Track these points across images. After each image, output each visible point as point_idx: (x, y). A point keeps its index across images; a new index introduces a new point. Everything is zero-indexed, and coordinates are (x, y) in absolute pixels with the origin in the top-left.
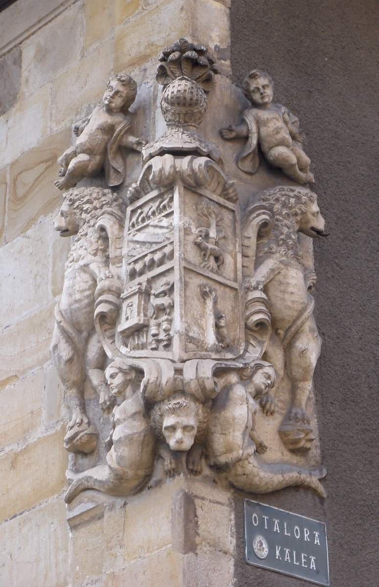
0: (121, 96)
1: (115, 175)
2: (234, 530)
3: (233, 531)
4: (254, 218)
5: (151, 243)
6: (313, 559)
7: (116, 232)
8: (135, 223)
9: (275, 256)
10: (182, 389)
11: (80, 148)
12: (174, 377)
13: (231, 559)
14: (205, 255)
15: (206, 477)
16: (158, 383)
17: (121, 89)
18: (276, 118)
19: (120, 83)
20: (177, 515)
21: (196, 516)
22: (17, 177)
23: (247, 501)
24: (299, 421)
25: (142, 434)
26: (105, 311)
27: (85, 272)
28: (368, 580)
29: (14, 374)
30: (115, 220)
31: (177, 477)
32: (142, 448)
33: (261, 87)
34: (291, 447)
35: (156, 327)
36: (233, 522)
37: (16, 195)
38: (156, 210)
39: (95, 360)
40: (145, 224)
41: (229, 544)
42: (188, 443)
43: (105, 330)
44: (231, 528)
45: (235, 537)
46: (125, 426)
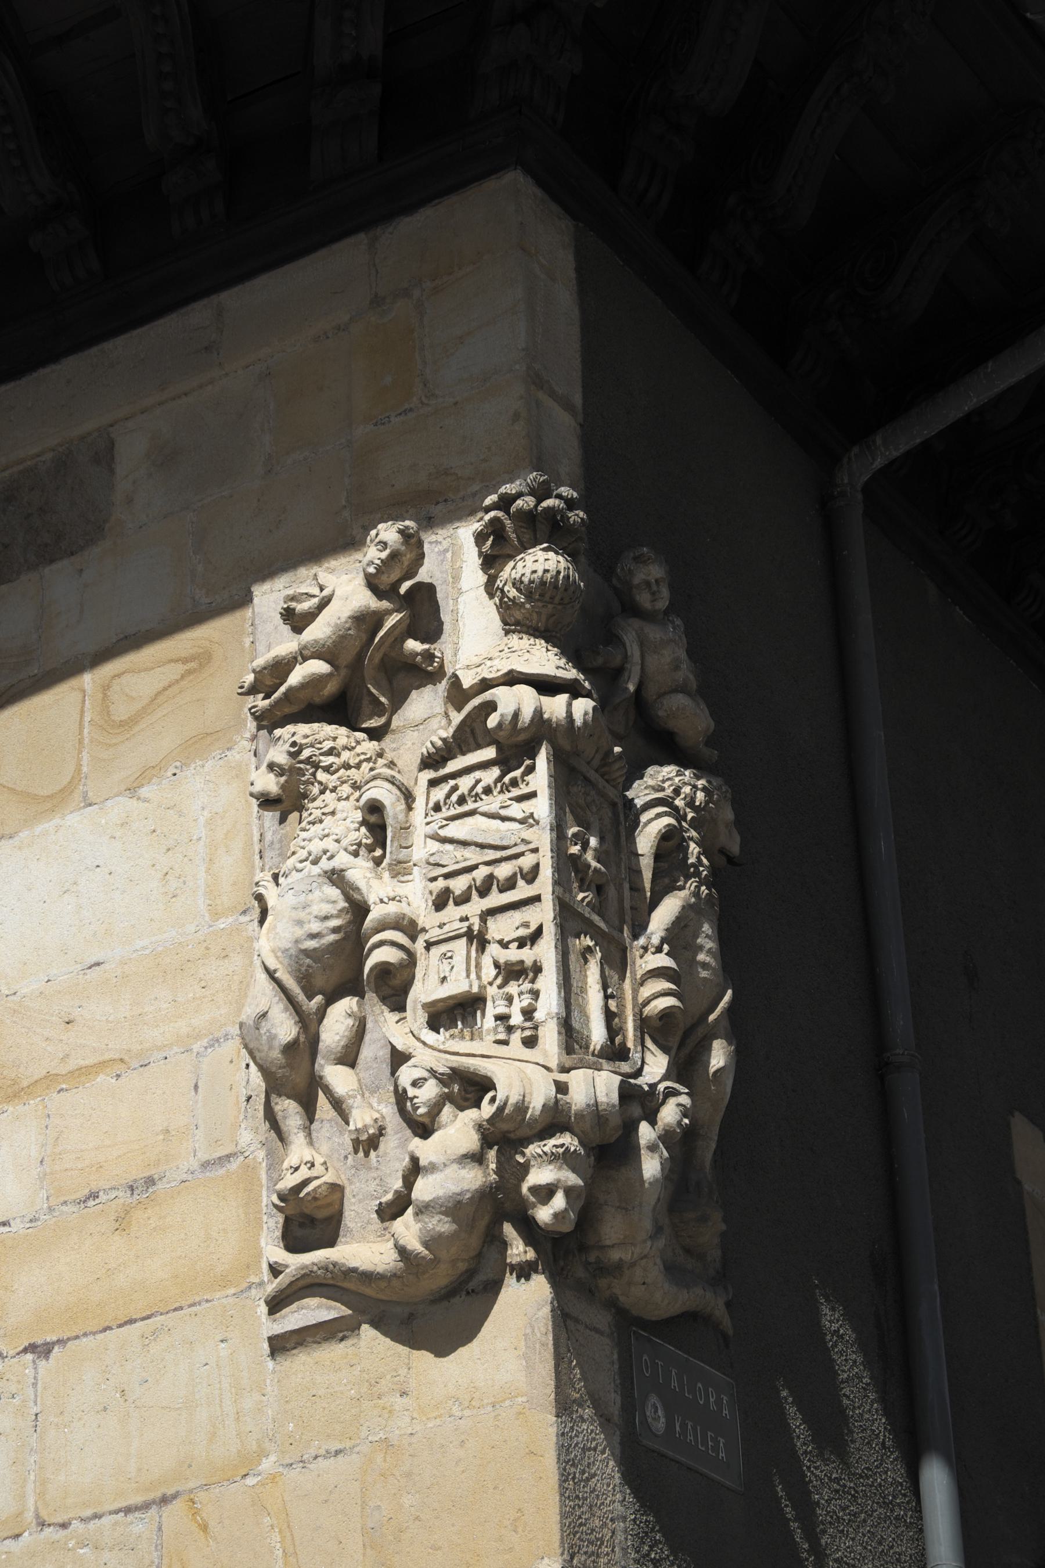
5: (482, 846)
6: (722, 1441)
7: (401, 817)
8: (442, 803)
12: (556, 1097)
13: (616, 1431)
20: (537, 1346)
26: (392, 961)
30: (398, 793)
35: (506, 1003)
36: (616, 1366)
38: (493, 785)
39: (339, 1049)
40: (466, 808)
41: (613, 1405)
44: (614, 1378)
45: (619, 1393)
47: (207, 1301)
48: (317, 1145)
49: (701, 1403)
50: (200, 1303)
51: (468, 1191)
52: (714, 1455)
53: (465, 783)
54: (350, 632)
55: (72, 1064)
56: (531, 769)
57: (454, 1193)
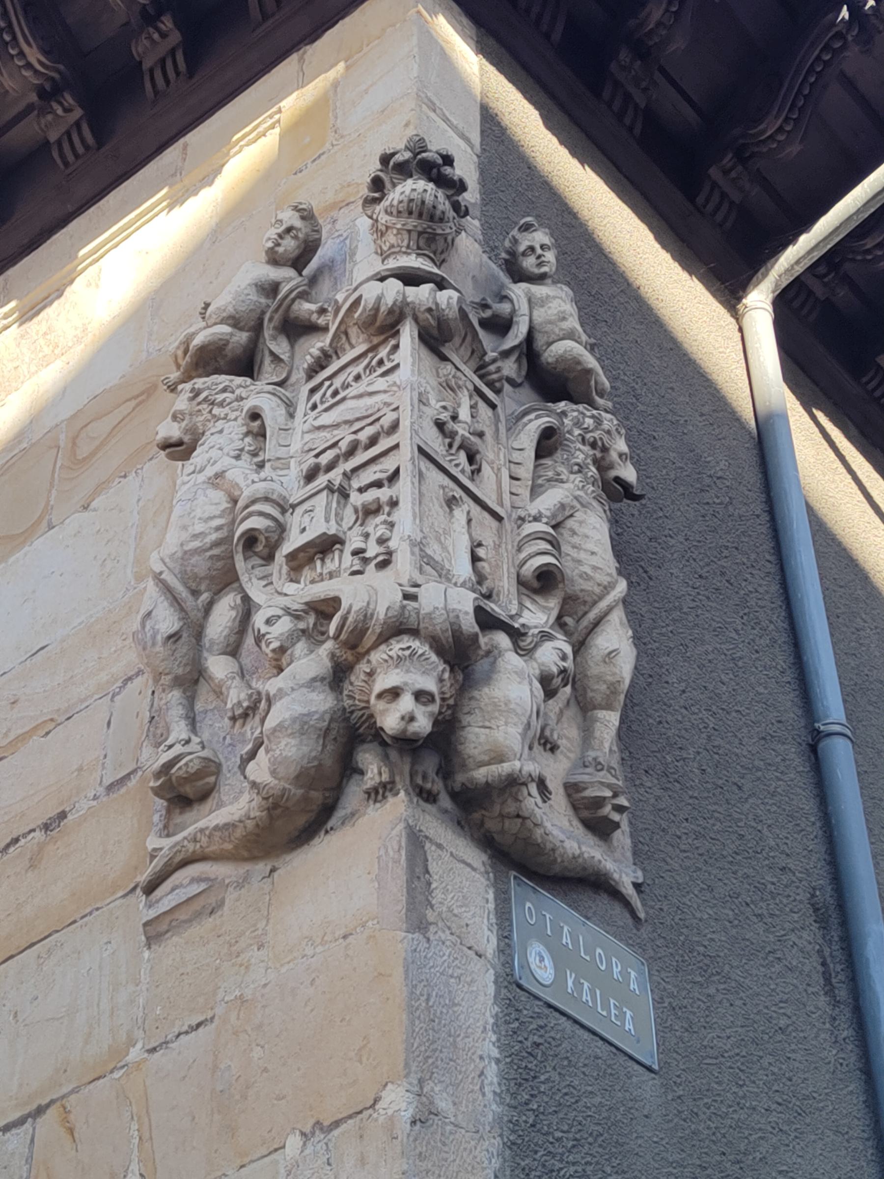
0: (296, 237)
1: (273, 366)
2: (493, 920)
3: (491, 921)
4: (530, 421)
6: (629, 1014)
9: (565, 486)
10: (416, 627)
11: (215, 317)
14: (450, 446)
15: (445, 811)
16: (370, 612)
17: (298, 223)
18: (561, 298)
19: (297, 214)
20: (390, 865)
21: (427, 872)
22: (79, 432)
23: (515, 877)
24: (602, 770)
25: (327, 717)
27: (216, 486)
28: (719, 1083)
29: (49, 717)
31: (391, 800)
32: (324, 746)
33: (538, 247)
34: (586, 814)
35: (362, 538)
36: (491, 906)
37: (75, 455)
39: (222, 639)
42: (423, 725)
43: (253, 568)
46: (294, 700)
47: (97, 909)
48: (199, 734)
49: (603, 968)
50: (91, 913)
51: (316, 712)
52: (588, 958)
53: (338, 382)
54: (249, 297)
55: (12, 736)
56: (396, 347)
57: (300, 714)
